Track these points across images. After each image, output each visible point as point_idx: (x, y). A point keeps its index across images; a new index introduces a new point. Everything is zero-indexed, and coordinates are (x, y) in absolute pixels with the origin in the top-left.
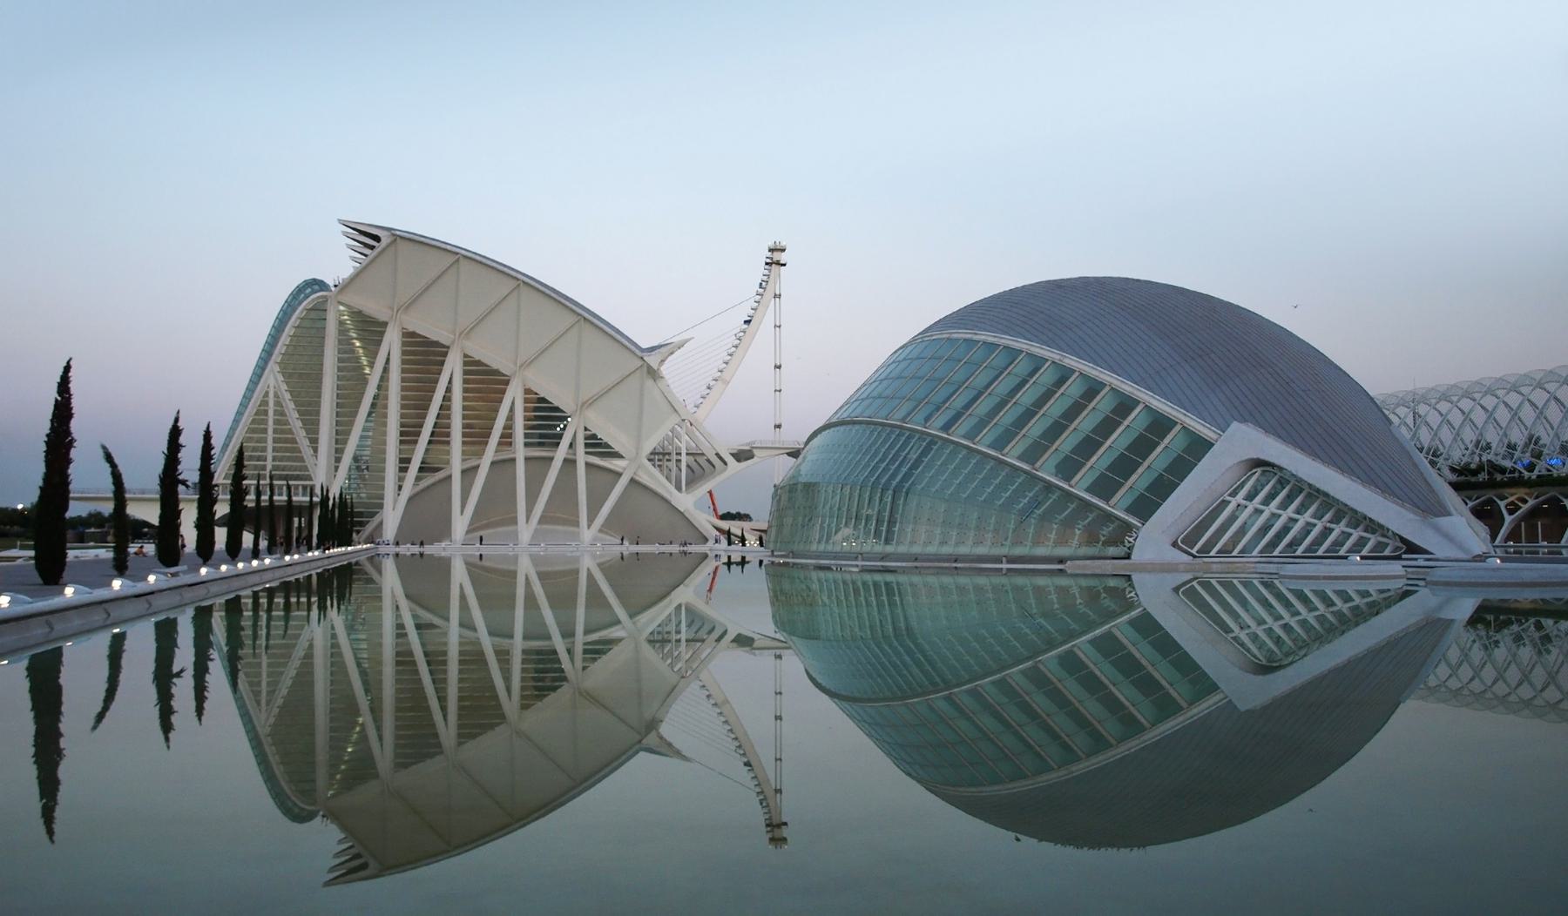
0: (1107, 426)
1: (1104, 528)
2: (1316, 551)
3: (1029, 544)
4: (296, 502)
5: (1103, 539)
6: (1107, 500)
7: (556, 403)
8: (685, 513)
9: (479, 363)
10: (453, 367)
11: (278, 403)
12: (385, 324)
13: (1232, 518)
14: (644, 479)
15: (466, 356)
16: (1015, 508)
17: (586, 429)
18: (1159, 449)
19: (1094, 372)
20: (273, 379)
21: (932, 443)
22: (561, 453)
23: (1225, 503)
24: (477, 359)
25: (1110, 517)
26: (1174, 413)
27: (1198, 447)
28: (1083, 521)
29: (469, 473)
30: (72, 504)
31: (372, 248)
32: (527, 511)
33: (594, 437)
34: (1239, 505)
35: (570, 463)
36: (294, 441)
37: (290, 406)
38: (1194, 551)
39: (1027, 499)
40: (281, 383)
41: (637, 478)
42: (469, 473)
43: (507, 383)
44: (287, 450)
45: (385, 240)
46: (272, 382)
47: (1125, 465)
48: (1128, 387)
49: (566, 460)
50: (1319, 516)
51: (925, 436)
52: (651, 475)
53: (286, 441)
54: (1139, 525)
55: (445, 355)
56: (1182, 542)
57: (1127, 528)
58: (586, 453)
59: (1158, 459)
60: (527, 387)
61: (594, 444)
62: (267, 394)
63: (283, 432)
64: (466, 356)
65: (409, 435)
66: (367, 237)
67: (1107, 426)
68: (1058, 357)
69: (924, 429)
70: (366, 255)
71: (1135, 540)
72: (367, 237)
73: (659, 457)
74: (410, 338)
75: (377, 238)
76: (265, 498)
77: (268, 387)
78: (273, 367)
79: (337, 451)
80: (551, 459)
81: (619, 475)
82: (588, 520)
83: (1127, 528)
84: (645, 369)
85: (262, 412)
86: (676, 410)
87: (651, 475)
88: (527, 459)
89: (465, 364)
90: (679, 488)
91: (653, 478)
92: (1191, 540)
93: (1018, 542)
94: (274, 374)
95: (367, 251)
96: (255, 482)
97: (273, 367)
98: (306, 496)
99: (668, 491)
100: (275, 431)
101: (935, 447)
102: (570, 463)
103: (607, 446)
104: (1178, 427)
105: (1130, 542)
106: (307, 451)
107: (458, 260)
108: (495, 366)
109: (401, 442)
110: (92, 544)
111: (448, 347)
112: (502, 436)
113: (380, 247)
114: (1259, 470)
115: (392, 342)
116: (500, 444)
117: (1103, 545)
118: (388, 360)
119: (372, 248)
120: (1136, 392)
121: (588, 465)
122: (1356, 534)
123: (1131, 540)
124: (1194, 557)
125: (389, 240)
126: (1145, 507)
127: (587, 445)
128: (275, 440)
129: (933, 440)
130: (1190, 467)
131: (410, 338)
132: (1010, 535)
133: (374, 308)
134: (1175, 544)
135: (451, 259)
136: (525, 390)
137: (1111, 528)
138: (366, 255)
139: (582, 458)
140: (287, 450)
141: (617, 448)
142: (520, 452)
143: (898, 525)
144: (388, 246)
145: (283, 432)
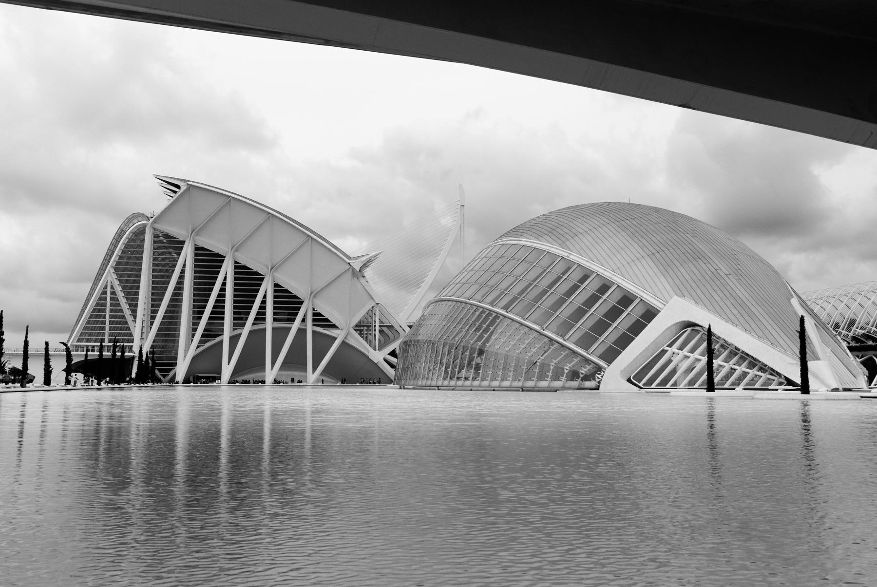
0: (592, 300)
1: (583, 369)
2: (723, 384)
3: (535, 379)
4: (126, 356)
5: (582, 376)
6: (586, 349)
7: (295, 293)
8: (378, 364)
9: (245, 267)
10: (227, 270)
11: (113, 293)
12: (183, 242)
13: (670, 361)
14: (351, 342)
15: (236, 262)
16: (528, 355)
17: (314, 309)
18: (624, 315)
19: (588, 264)
20: (110, 277)
21: (497, 317)
22: (296, 325)
23: (664, 352)
24: (243, 264)
25: (587, 361)
26: (636, 291)
27: (650, 314)
28: (569, 364)
29: (234, 340)
30: (73, 358)
31: (175, 192)
32: (272, 364)
33: (320, 314)
34: (674, 353)
35: (302, 332)
36: (124, 317)
37: (121, 295)
38: (641, 385)
39: (536, 349)
40: (115, 280)
41: (347, 341)
42: (234, 340)
43: (262, 279)
44: (120, 323)
45: (184, 187)
46: (109, 280)
47: (600, 327)
48: (608, 274)
49: (299, 329)
50: (738, 363)
51: (473, 306)
52: (357, 340)
53: (119, 317)
54: (606, 366)
55: (222, 261)
56: (633, 379)
57: (599, 369)
58: (314, 325)
59: (622, 323)
60: (276, 282)
61: (320, 319)
62: (106, 287)
63: (116, 311)
64: (236, 262)
65: (198, 313)
66: (173, 186)
67: (592, 300)
68: (566, 254)
69: (479, 303)
70: (172, 197)
71: (602, 377)
72: (173, 186)
73: (362, 328)
74: (199, 251)
75: (178, 187)
76: (119, 354)
77: (107, 283)
78: (110, 269)
79: (194, 324)
80: (290, 329)
81: (335, 339)
82: (313, 368)
83: (599, 369)
84: (351, 271)
85: (102, 298)
86: (372, 298)
87: (357, 340)
88: (274, 329)
89: (236, 267)
90: (375, 349)
91: (357, 342)
92: (639, 376)
93: (528, 379)
94: (111, 275)
95: (173, 195)
96: (99, 344)
97: (110, 269)
98: (83, 351)
99: (365, 348)
100: (111, 311)
101: (498, 321)
102: (302, 332)
103: (327, 320)
104: (638, 300)
105: (598, 378)
106: (130, 323)
107: (230, 201)
108: (255, 269)
109: (235, 319)
110: (358, 384)
111: (225, 257)
112: (258, 314)
113: (180, 192)
114: (689, 329)
115: (187, 254)
116: (256, 319)
117: (581, 380)
118: (184, 266)
119: (175, 192)
120: (612, 277)
121: (314, 332)
122: (753, 372)
123: (599, 376)
124: (641, 388)
125: (185, 188)
126: (610, 355)
127: (314, 320)
128: (111, 317)
129: (498, 315)
130: (644, 326)
131: (199, 251)
132: (523, 375)
133: (177, 232)
134: (629, 380)
135: (221, 201)
136: (275, 284)
137: (587, 369)
138: (172, 197)
139: (310, 327)
140: (120, 323)
141: (334, 321)
142: (269, 324)
143: (482, 369)
144: (185, 191)
145: (116, 311)
